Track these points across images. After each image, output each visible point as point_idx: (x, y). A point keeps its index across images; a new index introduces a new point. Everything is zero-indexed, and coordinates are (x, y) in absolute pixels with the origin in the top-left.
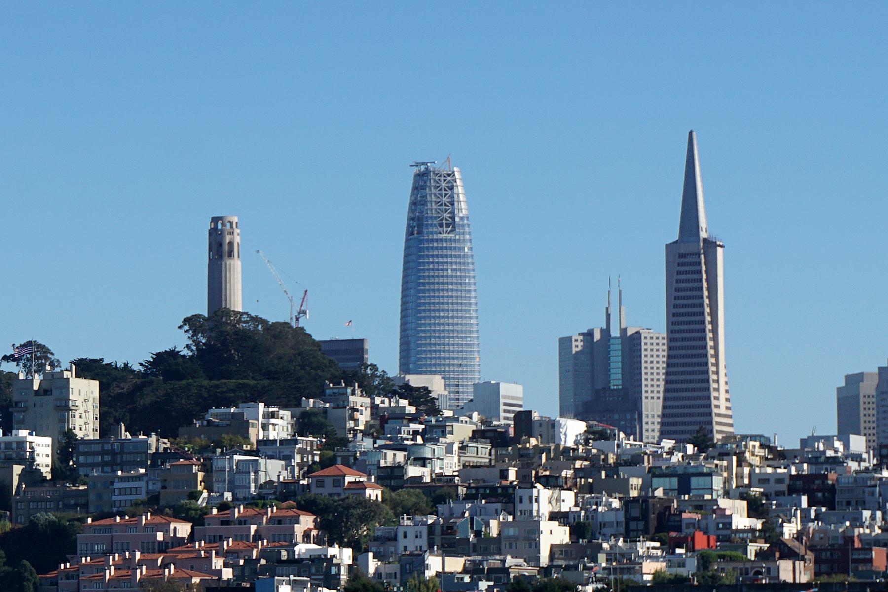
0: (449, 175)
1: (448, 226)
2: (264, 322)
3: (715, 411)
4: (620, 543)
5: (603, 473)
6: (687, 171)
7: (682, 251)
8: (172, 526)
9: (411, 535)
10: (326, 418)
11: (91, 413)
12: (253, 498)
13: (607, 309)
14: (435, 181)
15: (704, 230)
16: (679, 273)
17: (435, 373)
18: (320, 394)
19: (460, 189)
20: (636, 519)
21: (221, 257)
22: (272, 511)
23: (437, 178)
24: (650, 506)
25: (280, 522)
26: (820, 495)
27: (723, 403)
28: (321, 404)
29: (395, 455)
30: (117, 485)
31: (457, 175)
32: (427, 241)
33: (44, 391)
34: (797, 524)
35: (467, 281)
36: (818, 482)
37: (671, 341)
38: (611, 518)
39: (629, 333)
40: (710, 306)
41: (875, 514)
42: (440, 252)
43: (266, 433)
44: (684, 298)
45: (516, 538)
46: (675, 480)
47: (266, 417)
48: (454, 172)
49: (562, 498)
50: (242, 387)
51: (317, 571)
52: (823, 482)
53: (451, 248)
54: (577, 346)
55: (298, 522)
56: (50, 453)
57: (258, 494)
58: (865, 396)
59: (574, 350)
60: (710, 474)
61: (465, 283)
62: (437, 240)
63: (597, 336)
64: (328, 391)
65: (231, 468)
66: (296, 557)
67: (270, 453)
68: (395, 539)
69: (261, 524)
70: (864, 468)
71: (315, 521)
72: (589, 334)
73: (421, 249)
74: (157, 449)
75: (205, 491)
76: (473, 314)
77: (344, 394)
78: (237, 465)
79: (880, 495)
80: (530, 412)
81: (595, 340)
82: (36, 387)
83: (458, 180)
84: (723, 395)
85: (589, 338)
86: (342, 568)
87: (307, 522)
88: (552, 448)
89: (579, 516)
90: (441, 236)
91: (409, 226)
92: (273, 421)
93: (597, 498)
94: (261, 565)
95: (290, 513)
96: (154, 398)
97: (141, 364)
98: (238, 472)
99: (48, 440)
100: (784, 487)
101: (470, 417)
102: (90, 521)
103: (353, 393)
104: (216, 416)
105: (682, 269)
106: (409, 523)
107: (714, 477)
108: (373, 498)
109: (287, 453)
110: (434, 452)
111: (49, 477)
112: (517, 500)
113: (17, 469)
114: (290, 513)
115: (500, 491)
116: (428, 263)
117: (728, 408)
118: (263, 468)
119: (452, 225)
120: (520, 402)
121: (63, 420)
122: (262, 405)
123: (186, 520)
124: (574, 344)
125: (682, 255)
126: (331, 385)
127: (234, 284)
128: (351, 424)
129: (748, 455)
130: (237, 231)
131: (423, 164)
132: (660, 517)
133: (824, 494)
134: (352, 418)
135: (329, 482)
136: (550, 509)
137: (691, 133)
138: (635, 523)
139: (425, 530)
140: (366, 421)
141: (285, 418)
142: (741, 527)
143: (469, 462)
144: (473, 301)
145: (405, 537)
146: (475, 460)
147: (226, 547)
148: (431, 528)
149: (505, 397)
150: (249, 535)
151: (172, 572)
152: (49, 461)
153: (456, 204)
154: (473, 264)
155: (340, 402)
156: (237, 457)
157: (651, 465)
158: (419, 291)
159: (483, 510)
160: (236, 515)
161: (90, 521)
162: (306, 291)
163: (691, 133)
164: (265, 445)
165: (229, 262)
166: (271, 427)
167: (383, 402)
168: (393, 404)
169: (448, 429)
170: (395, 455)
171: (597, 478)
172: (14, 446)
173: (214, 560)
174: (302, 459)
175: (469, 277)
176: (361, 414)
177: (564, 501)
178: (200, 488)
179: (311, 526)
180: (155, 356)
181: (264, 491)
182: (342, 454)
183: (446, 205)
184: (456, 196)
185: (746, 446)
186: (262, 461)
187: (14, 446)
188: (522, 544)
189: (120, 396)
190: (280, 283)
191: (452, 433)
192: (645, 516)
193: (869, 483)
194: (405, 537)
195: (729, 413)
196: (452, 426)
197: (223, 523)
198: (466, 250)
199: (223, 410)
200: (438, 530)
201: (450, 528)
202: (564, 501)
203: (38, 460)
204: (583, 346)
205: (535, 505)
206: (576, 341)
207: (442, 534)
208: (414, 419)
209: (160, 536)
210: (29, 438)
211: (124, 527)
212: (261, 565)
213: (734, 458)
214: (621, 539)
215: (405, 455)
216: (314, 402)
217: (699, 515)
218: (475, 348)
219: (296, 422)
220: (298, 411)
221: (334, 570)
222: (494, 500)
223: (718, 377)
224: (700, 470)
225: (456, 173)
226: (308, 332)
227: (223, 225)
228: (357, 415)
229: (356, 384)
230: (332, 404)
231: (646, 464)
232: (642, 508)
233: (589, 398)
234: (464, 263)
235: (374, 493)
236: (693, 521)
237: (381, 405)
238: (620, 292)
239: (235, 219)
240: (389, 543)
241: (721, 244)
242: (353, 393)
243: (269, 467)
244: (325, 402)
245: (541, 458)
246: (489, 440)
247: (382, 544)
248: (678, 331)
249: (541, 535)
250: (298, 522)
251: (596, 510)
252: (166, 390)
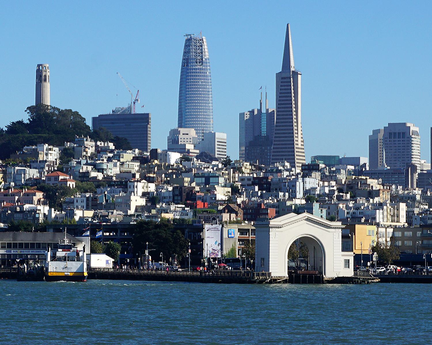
0: (201, 40)
1: (200, 62)
2: (58, 109)
3: (296, 146)
4: (164, 205)
5: (174, 176)
6: (286, 43)
9: (79, 201)
10: (74, 151)
12: (23, 185)
13: (260, 100)
14: (194, 43)
15: (293, 67)
16: (281, 86)
17: (191, 127)
19: (205, 47)
20: (177, 195)
21: (41, 81)
22: (25, 191)
23: (195, 41)
25: (28, 195)
26: (265, 186)
27: (300, 143)
28: (73, 145)
29: (87, 167)
31: (204, 40)
32: (190, 69)
34: (244, 198)
35: (208, 87)
36: (265, 180)
37: (278, 112)
39: (269, 112)
40: (295, 100)
41: (285, 194)
43: (47, 157)
45: (121, 203)
46: (204, 179)
47: (47, 150)
48: (203, 39)
49: (149, 186)
50: (40, 137)
52: (267, 180)
53: (201, 73)
54: (247, 117)
55: (35, 195)
57: (25, 183)
58: (380, 139)
59: (245, 118)
60: (218, 177)
61: (207, 88)
63: (256, 112)
64: (76, 140)
65: (14, 172)
66: (24, 210)
67: (35, 166)
68: (73, 203)
69: (20, 196)
70: (313, 175)
71: (43, 195)
72: (252, 112)
73: (188, 73)
75: (3, 182)
76: (211, 102)
77: (82, 141)
78: (17, 171)
80: (157, 149)
81: (255, 114)
83: (204, 42)
84: (300, 139)
85: (252, 113)
86: (40, 215)
87: (39, 195)
88: (163, 165)
89: (154, 194)
90: (196, 67)
92: (50, 152)
93: (162, 186)
94: (8, 213)
95: (33, 191)
96: (4, 142)
97: (6, 127)
98: (17, 173)
100: (250, 182)
103: (87, 140)
104: (27, 150)
106: (80, 196)
107: (219, 178)
108: (71, 186)
109: (42, 166)
110: (108, 166)
112: (128, 187)
114: (33, 191)
116: (191, 79)
117: (302, 145)
118: (28, 172)
119: (201, 62)
125: (282, 78)
126: (78, 137)
127: (46, 93)
129: (243, 168)
131: (189, 35)
132: (188, 194)
133: (267, 186)
134: (85, 151)
135: (53, 178)
136: (143, 190)
137: (288, 25)
138: (177, 197)
139: (85, 199)
140: (91, 153)
141: (56, 151)
142: (220, 199)
143: (123, 170)
145: (77, 202)
146: (128, 169)
147: (2, 205)
148: (88, 199)
149: (218, 138)
150: (15, 200)
153: (203, 53)
154: (211, 79)
155: (81, 144)
156: (17, 168)
157: (196, 172)
159: (114, 191)
160: (10, 192)
162: (138, 91)
163: (288, 25)
164: (34, 163)
166: (49, 154)
167: (101, 144)
168: (106, 145)
169: (121, 156)
170: (87, 167)
174: (49, 169)
175: (209, 85)
176: (89, 149)
177: (149, 187)
179: (42, 197)
180: (11, 124)
181: (28, 182)
182: (65, 167)
183: (199, 53)
184: (203, 49)
185: (243, 165)
188: (123, 206)
190: (127, 87)
191: (123, 158)
192: (181, 194)
194: (77, 202)
195: (303, 147)
196: (123, 155)
197: (5, 195)
198: (208, 73)
199: (30, 147)
200: (90, 199)
201: (96, 198)
202: (149, 187)
204: (250, 117)
205: (136, 189)
206: (246, 114)
208: (112, 151)
212: (8, 213)
213: (232, 170)
215: (92, 168)
216: (70, 144)
217: (203, 194)
218: (211, 117)
220: (62, 148)
222: (119, 187)
223: (298, 132)
224: (215, 175)
225: (204, 39)
228: (87, 150)
229: (88, 136)
230: (77, 145)
231: (193, 172)
232: (180, 190)
233: (252, 140)
234: (206, 79)
235: (71, 184)
236: (200, 197)
237: (100, 145)
238: (266, 93)
239: (47, 65)
240: (70, 204)
241: (300, 73)
242: (87, 140)
243: (31, 172)
244: (74, 144)
245: (155, 169)
246: (139, 161)
247: (68, 205)
248: (281, 111)
249: (131, 202)
250: (35, 195)
251: (161, 191)
252: (9, 138)
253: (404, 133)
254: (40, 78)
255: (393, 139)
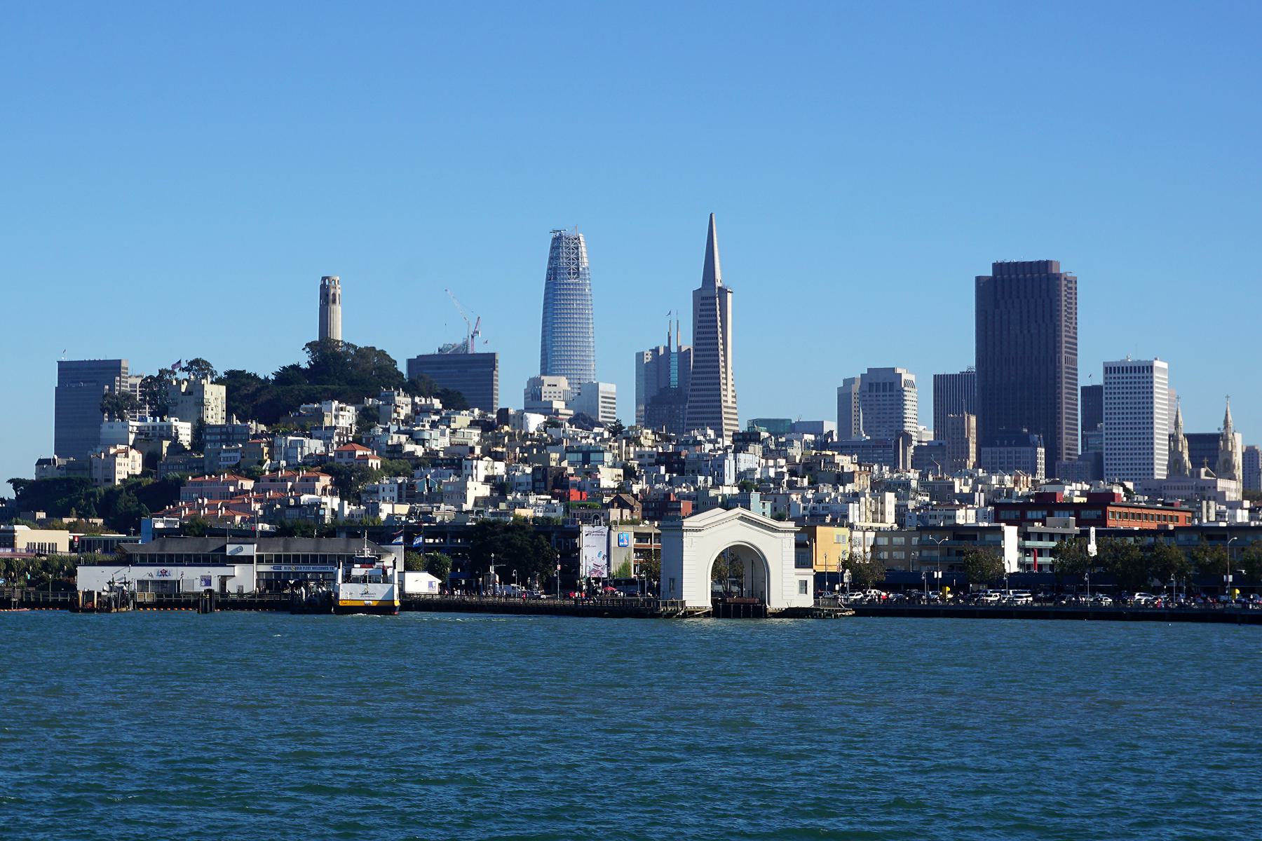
1: (574, 274)
3: (724, 404)
4: (519, 496)
5: (535, 450)
7: (704, 296)
8: (240, 483)
10: (379, 411)
11: (220, 407)
16: (701, 310)
17: (561, 375)
18: (376, 396)
19: (583, 249)
20: (539, 481)
21: (327, 303)
24: (548, 472)
25: (307, 481)
26: (676, 466)
27: (730, 399)
28: (377, 402)
30: (222, 455)
32: (560, 284)
33: (189, 392)
36: (675, 457)
38: (523, 480)
39: (683, 350)
40: (722, 333)
42: (569, 292)
44: (704, 327)
45: (452, 493)
51: (311, 513)
54: (648, 358)
56: (190, 433)
60: (603, 452)
62: (566, 284)
63: (662, 352)
64: (382, 394)
65: (286, 445)
67: (318, 435)
69: (295, 481)
71: (331, 480)
72: (657, 350)
74: (256, 431)
76: (592, 335)
78: (290, 443)
79: (712, 466)
82: (183, 390)
84: (730, 394)
87: (325, 480)
91: (548, 274)
92: (341, 413)
95: (314, 474)
99: (189, 425)
100: (653, 461)
101: (473, 412)
102: (190, 478)
103: (399, 395)
104: (305, 409)
105: (703, 307)
111: (189, 448)
112: (464, 467)
113: (166, 444)
114: (314, 474)
115: (456, 461)
117: (733, 402)
118: (307, 445)
119: (577, 273)
120: (614, 396)
121: (200, 412)
122: (336, 402)
123: (251, 478)
124: (645, 357)
125: (703, 298)
128: (395, 415)
129: (642, 438)
130: (339, 286)
132: (556, 479)
134: (395, 411)
136: (486, 473)
137: (711, 215)
139: (396, 487)
142: (605, 487)
144: (591, 326)
148: (400, 486)
149: (603, 392)
151: (224, 512)
152: (189, 438)
155: (390, 400)
158: (554, 319)
161: (190, 478)
163: (711, 215)
165: (333, 307)
167: (421, 401)
168: (428, 402)
171: (531, 453)
172: (165, 428)
173: (253, 505)
174: (340, 439)
178: (265, 458)
179: (328, 483)
181: (307, 460)
185: (641, 433)
186: (306, 440)
187: (165, 428)
188: (455, 496)
189: (247, 396)
192: (545, 479)
193: (705, 458)
195: (734, 405)
197: (271, 481)
200: (404, 487)
201: (413, 485)
203: (181, 438)
204: (652, 359)
205: (475, 471)
207: (407, 489)
209: (232, 489)
210: (175, 424)
211: (210, 482)
213: (624, 441)
214: (519, 494)
219: (359, 414)
220: (361, 406)
221: (321, 512)
226: (388, 353)
227: (329, 282)
228: (399, 409)
231: (565, 444)
233: (655, 394)
235: (375, 463)
242: (399, 395)
248: (700, 350)
253: (891, 384)
254: (327, 298)
255: (881, 393)
